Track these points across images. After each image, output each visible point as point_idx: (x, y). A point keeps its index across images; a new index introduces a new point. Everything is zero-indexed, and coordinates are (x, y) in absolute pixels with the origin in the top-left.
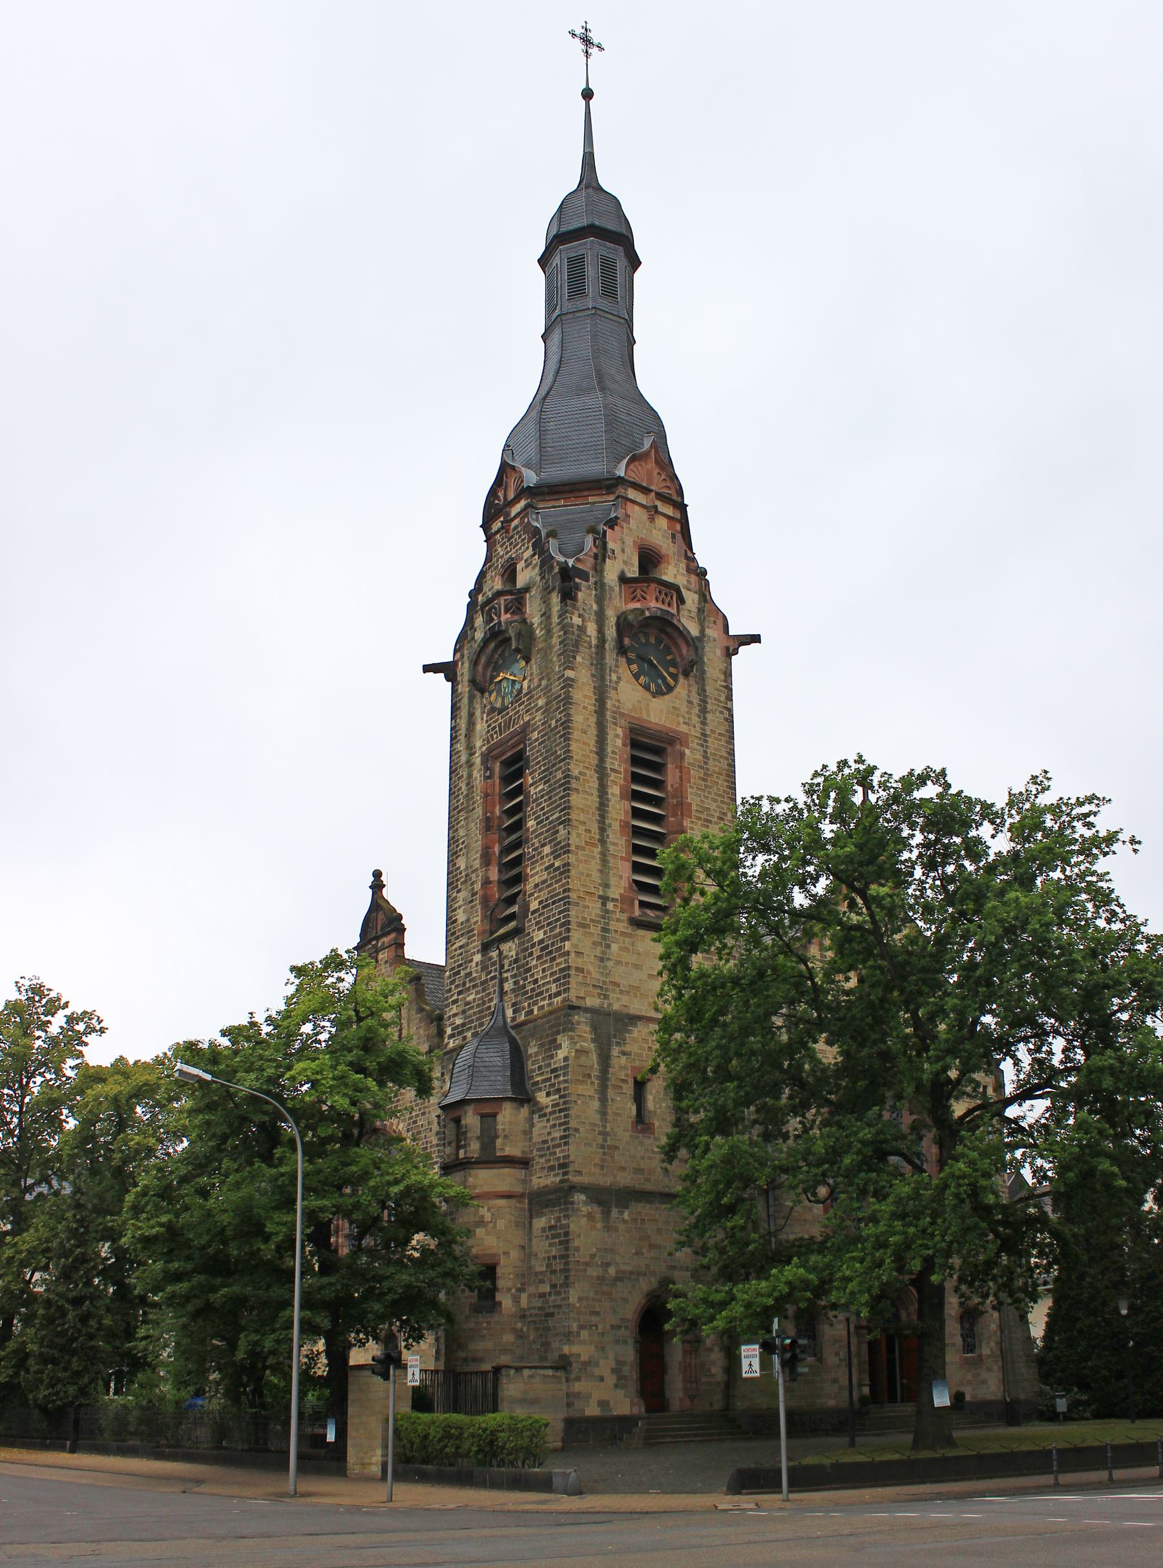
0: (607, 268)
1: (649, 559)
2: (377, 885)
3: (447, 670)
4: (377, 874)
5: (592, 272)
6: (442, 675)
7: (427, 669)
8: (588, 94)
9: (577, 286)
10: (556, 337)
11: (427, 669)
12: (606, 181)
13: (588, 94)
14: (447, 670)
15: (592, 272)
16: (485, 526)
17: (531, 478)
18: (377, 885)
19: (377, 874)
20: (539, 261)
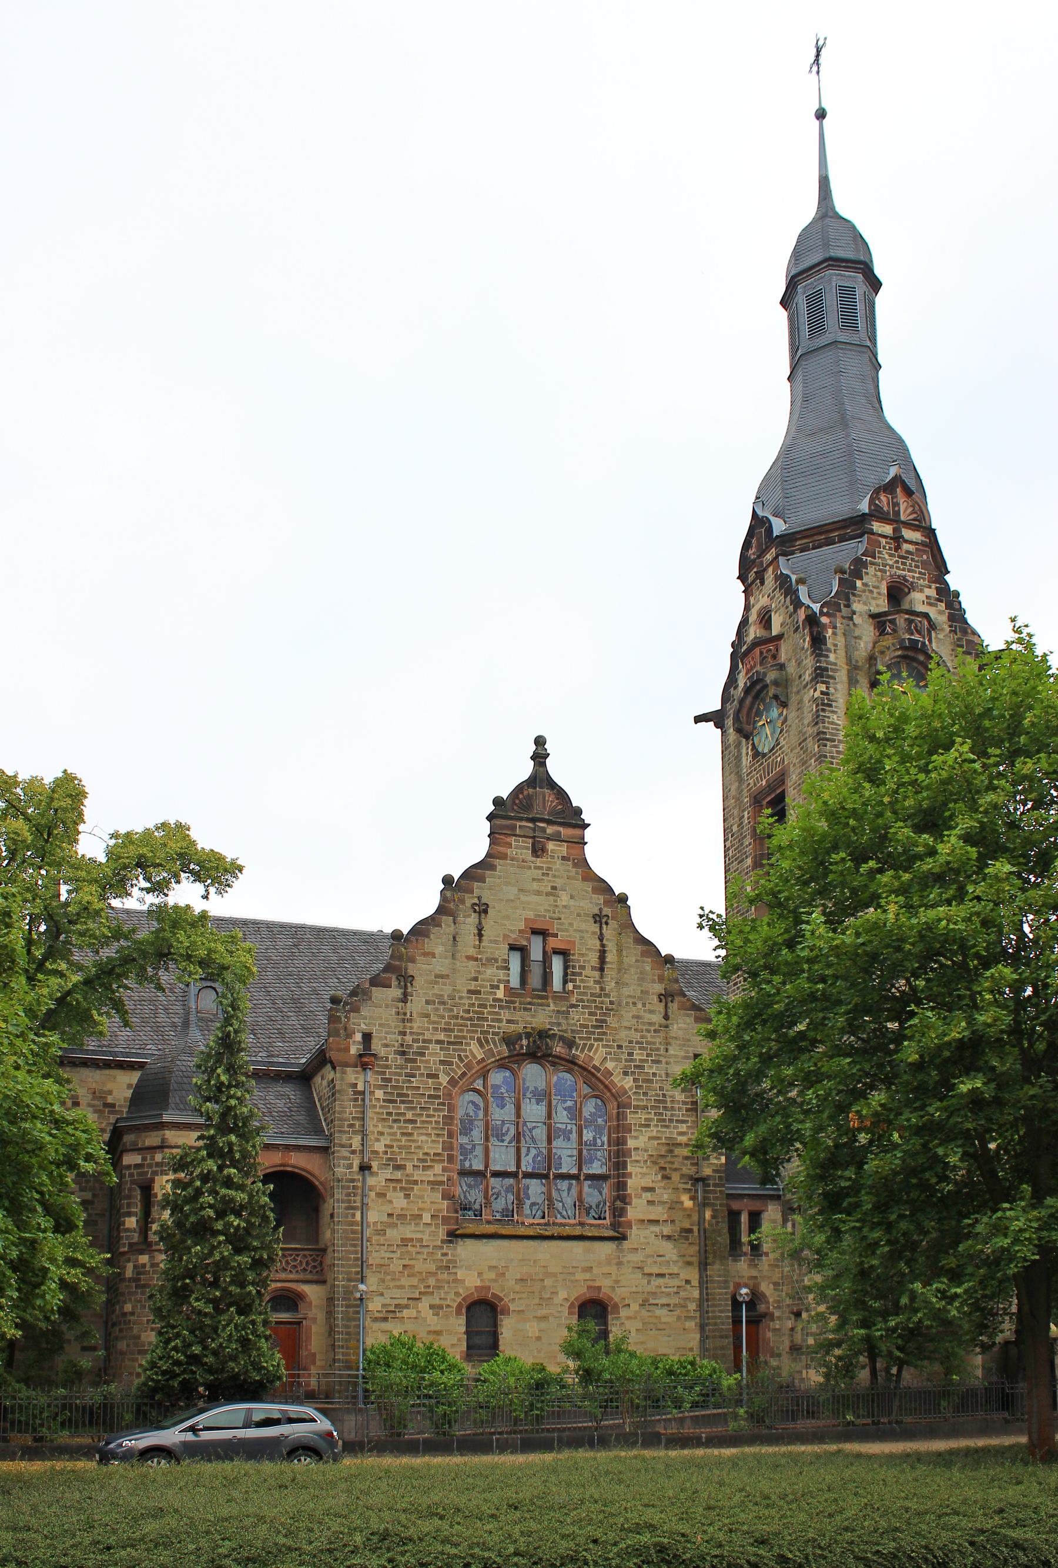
0: (847, 294)
1: (897, 593)
2: (540, 757)
3: (716, 718)
4: (540, 741)
5: (831, 302)
6: (712, 723)
7: (698, 719)
8: (821, 115)
9: (817, 326)
10: (801, 300)
11: (698, 719)
12: (843, 206)
13: (821, 115)
14: (716, 718)
15: (831, 302)
16: (742, 577)
17: (779, 527)
18: (540, 757)
19: (540, 741)
20: (781, 303)
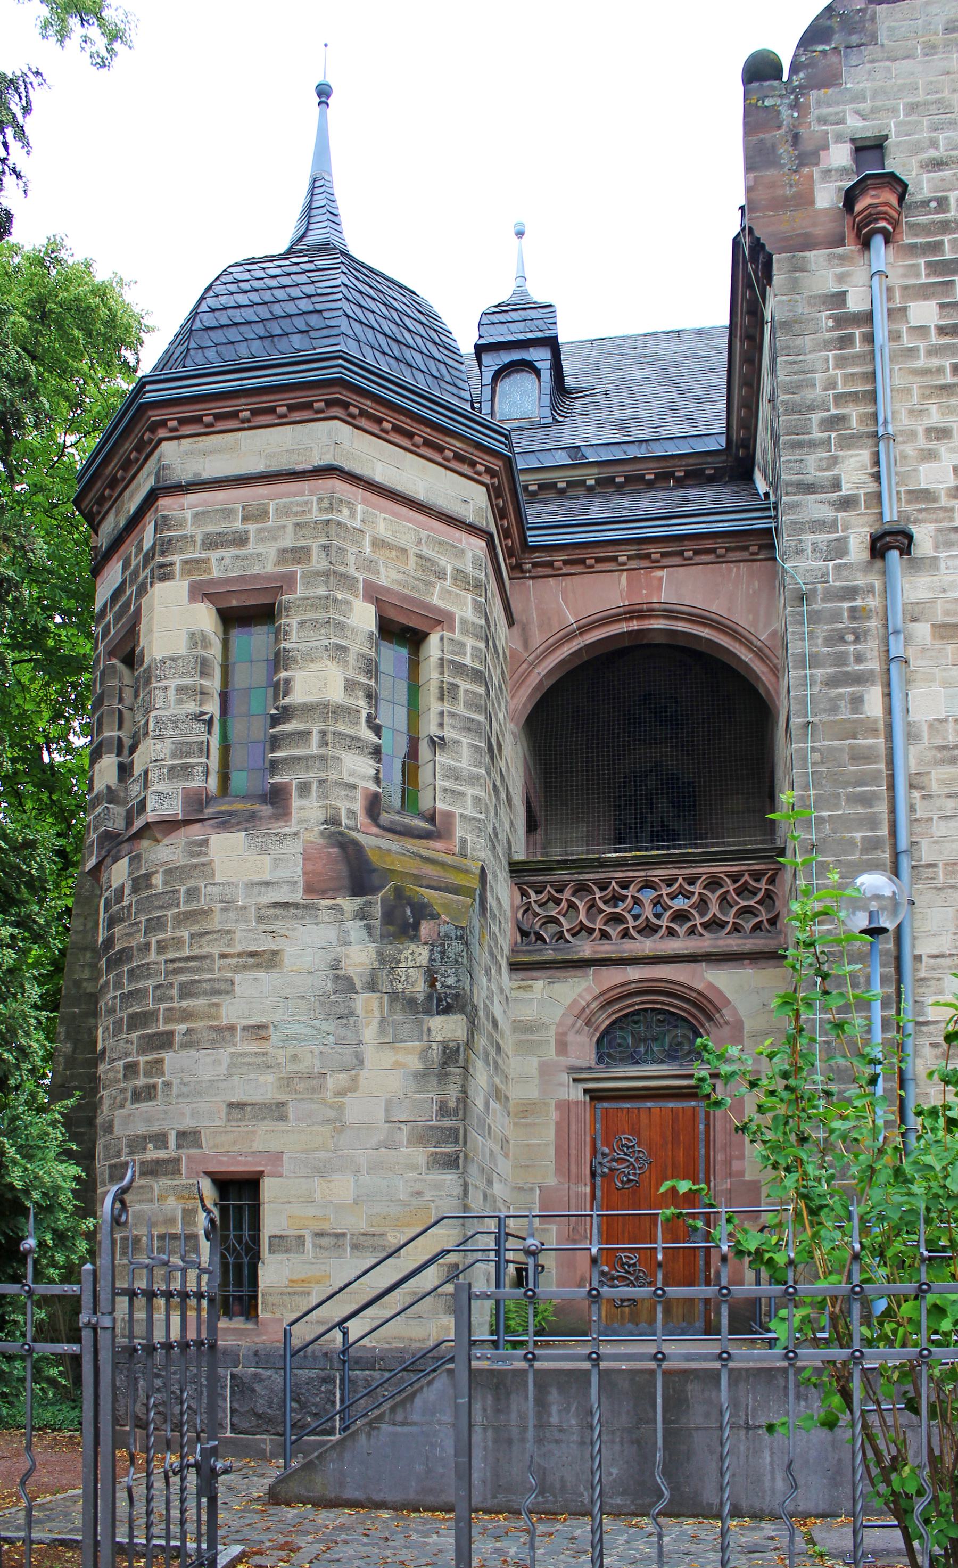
8: (324, 93)
13: (324, 93)
